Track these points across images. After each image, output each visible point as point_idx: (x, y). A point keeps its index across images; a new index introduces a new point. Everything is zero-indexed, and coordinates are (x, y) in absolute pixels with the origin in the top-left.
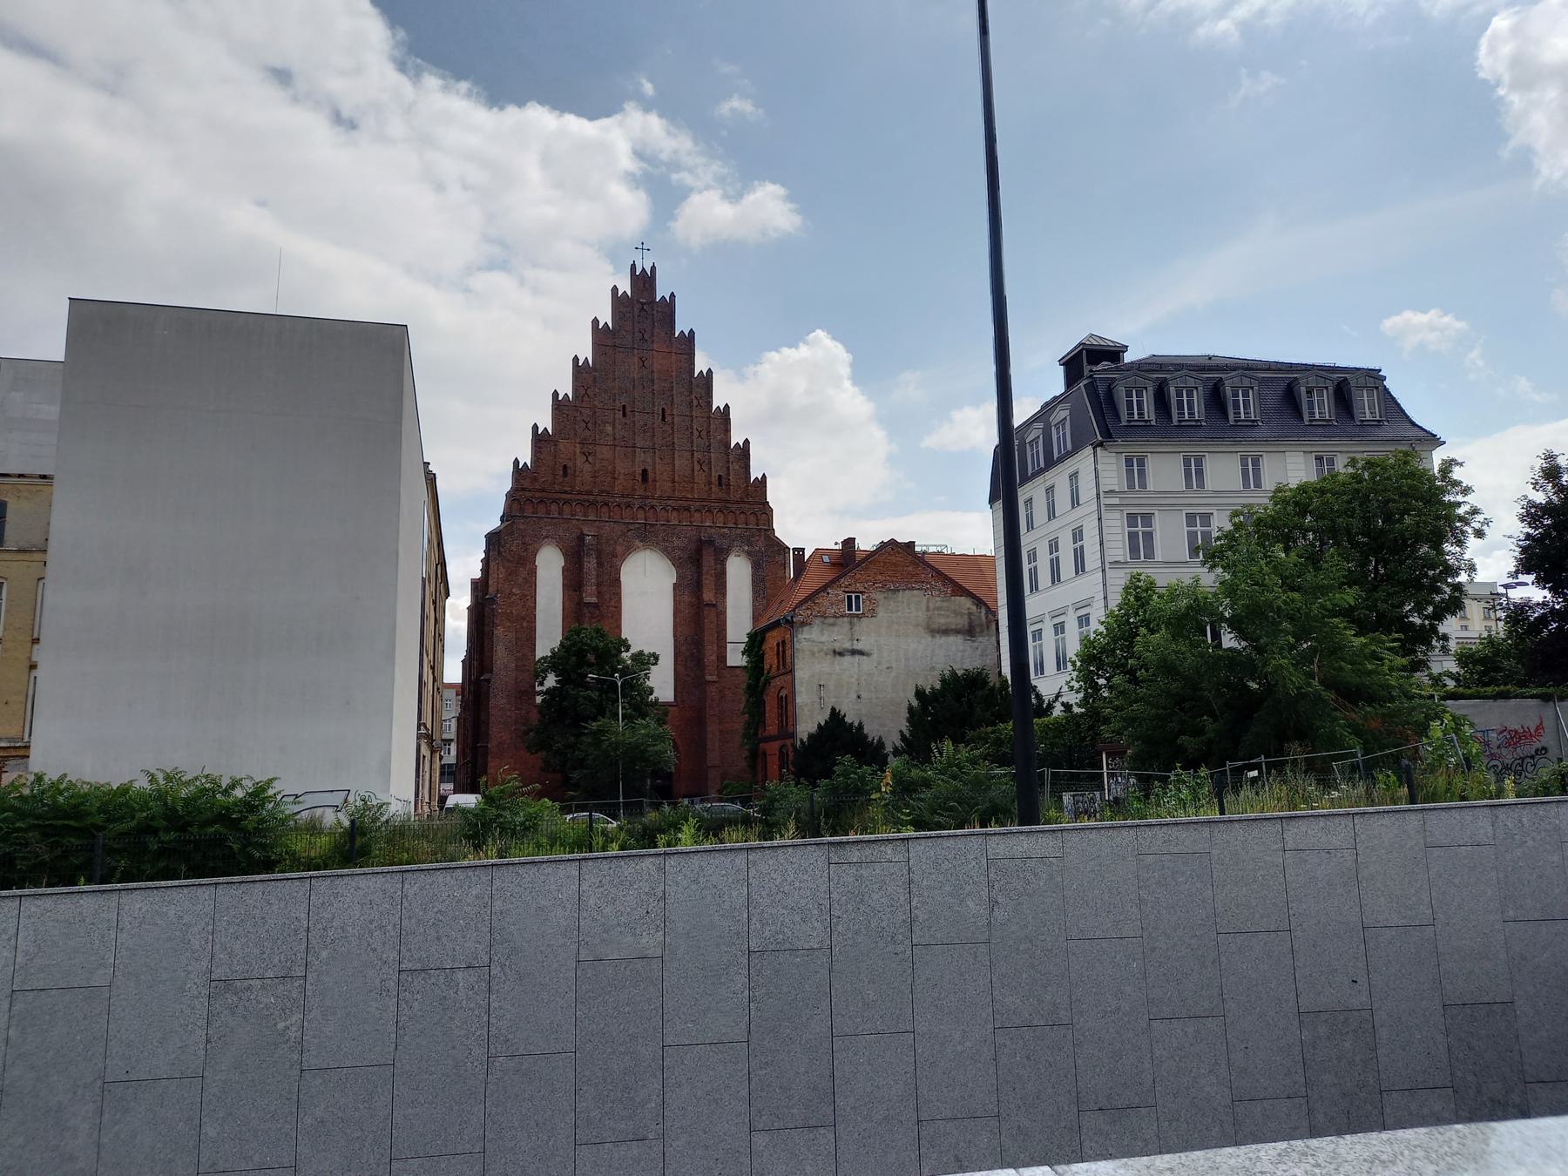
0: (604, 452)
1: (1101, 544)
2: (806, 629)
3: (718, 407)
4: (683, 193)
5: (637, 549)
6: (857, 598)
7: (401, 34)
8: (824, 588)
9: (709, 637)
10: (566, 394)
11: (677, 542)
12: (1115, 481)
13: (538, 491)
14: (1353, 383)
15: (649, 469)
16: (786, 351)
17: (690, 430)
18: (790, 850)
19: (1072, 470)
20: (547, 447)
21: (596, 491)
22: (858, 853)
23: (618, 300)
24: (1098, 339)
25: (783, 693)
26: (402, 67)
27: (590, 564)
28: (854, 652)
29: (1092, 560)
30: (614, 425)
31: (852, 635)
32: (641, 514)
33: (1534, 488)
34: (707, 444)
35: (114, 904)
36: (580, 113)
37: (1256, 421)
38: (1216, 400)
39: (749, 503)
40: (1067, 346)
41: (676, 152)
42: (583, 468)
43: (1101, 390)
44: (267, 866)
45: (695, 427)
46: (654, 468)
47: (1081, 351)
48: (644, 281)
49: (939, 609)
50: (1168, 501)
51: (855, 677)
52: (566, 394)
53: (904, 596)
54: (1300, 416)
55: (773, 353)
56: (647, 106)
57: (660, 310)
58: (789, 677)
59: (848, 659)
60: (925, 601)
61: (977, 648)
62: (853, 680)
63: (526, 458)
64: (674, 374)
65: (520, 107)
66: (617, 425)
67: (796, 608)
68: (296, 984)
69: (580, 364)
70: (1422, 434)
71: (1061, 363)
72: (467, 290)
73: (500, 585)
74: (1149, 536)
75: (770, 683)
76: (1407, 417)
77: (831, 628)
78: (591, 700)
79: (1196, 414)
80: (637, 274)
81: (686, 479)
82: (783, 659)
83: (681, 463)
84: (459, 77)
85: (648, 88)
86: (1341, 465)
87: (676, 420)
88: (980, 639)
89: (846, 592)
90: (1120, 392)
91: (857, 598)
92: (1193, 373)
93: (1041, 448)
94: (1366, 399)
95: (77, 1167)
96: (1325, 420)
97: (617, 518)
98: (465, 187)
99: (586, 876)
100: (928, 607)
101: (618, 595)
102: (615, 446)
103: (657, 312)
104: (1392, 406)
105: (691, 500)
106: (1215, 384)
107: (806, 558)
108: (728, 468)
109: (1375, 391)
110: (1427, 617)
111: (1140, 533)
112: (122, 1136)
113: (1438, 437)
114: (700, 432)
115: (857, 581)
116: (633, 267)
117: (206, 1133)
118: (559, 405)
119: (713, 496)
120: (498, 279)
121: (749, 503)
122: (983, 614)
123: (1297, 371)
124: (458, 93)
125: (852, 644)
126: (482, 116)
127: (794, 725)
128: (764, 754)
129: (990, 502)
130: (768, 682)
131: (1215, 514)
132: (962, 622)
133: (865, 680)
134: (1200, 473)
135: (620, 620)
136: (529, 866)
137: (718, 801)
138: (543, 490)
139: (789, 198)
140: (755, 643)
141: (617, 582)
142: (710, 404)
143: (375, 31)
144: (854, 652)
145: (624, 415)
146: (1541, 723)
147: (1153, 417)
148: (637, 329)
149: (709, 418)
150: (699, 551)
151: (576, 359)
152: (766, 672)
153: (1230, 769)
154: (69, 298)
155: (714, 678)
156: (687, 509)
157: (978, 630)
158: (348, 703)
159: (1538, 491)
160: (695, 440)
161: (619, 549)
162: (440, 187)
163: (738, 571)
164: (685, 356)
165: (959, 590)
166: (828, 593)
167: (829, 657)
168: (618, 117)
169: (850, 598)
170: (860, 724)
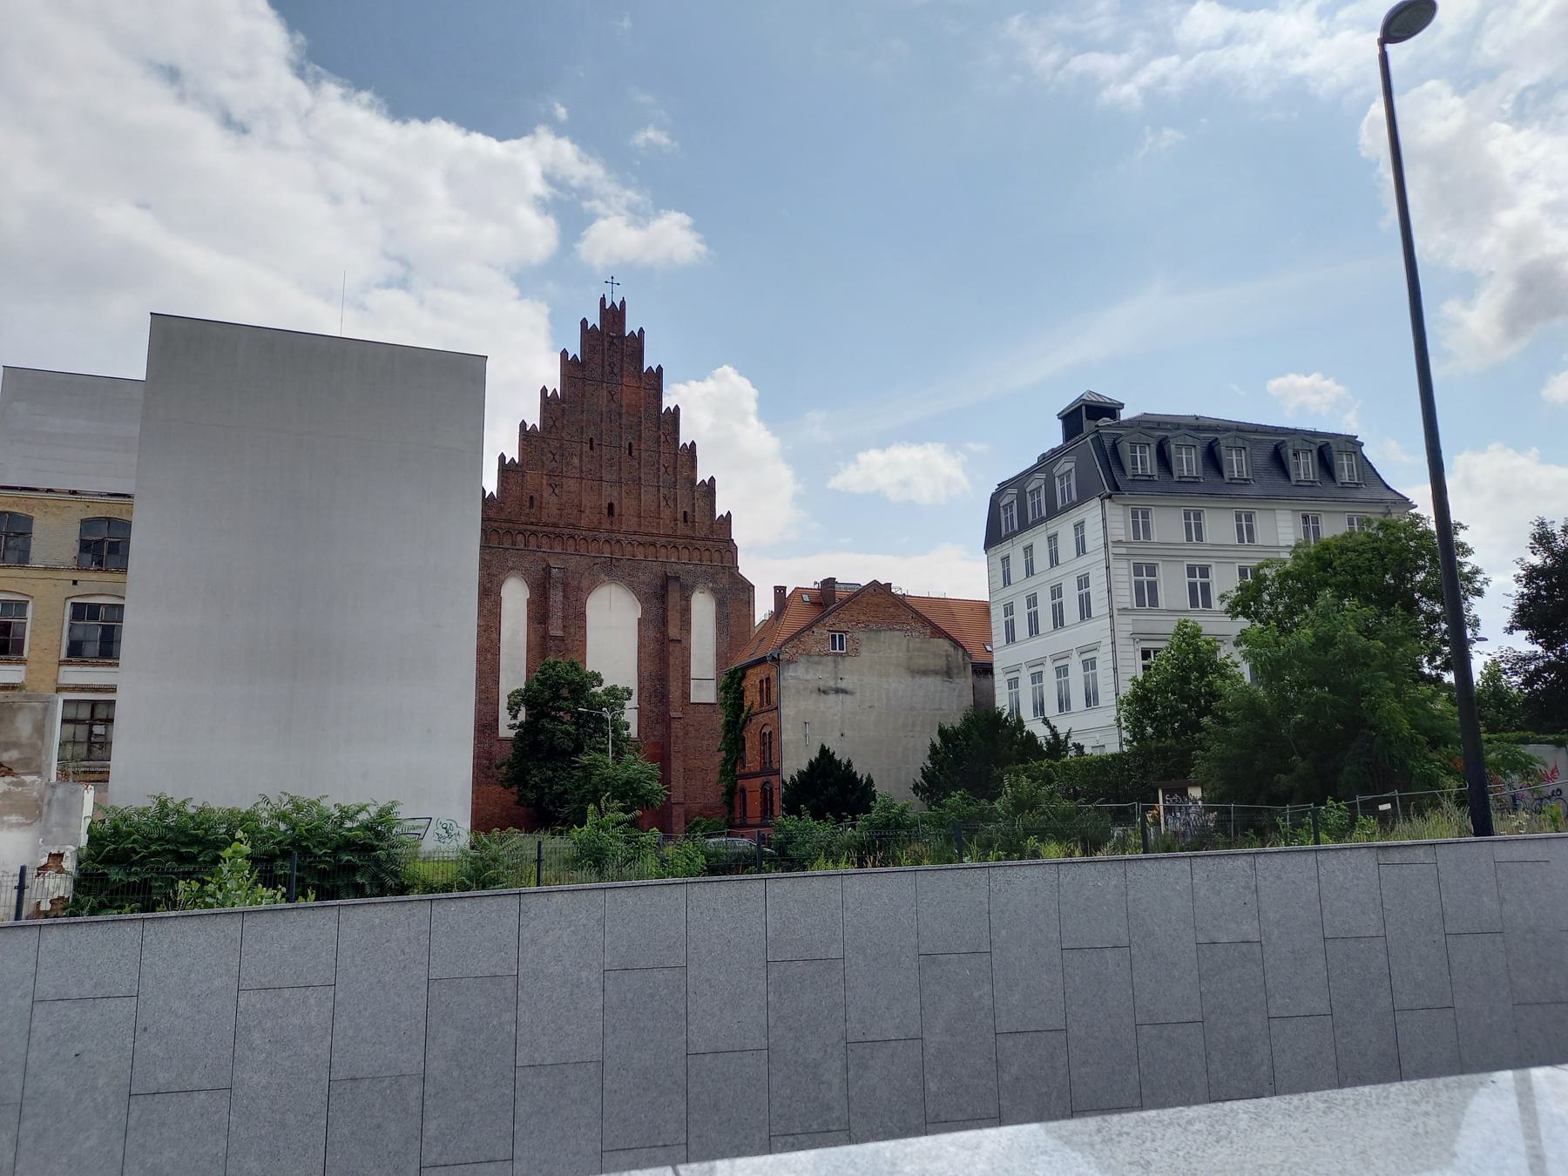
0: (571, 485)
1: (1109, 591)
2: (792, 666)
3: (685, 444)
4: (591, 218)
6: (841, 637)
7: (300, 38)
8: (809, 627)
9: (674, 675)
12: (1123, 532)
13: (506, 521)
14: (1334, 447)
17: (657, 466)
18: (1348, 852)
19: (1077, 520)
22: (1398, 855)
24: (1096, 396)
25: (766, 730)
26: (300, 72)
27: (556, 597)
28: (838, 691)
29: (1099, 605)
30: (581, 457)
32: (607, 548)
33: (1533, 552)
34: (673, 479)
35: (839, 887)
36: (488, 132)
37: (1249, 480)
38: (1212, 459)
40: (1066, 401)
41: (587, 179)
42: (551, 500)
43: (1108, 444)
44: (403, 890)
48: (613, 315)
49: (919, 650)
50: (1171, 553)
51: (839, 715)
53: (885, 636)
54: (1288, 477)
55: (682, 386)
56: (559, 131)
58: (775, 714)
59: (832, 697)
60: (905, 641)
61: (954, 690)
62: (836, 718)
64: (642, 409)
66: (584, 457)
67: (782, 645)
68: (985, 959)
69: (549, 395)
70: (1397, 498)
71: (1060, 416)
72: (362, 307)
74: (1153, 587)
75: (751, 720)
76: (1383, 481)
78: (568, 733)
80: (607, 307)
81: (652, 515)
82: (767, 696)
83: (648, 498)
84: (359, 85)
85: (561, 112)
88: (957, 680)
92: (1192, 432)
93: (1043, 497)
94: (1345, 462)
95: (834, 1115)
96: (1193, 477)
98: (364, 200)
99: (1197, 871)
100: (908, 647)
104: (1368, 473)
105: (657, 535)
106: (1276, 446)
107: (787, 596)
109: (1243, 451)
110: (1436, 668)
112: (866, 1090)
113: (1410, 501)
114: (666, 468)
115: (841, 620)
116: (603, 300)
117: (928, 1089)
120: (395, 296)
122: (960, 656)
123: (1283, 434)
125: (836, 683)
126: (384, 129)
127: (780, 761)
128: (743, 790)
129: (985, 548)
130: (749, 718)
131: (1160, 565)
132: (941, 663)
133: (849, 718)
134: (1250, 530)
135: (585, 654)
136: (1152, 861)
138: (510, 521)
139: (695, 228)
140: (732, 683)
141: (582, 616)
142: (677, 440)
143: (272, 34)
144: (838, 691)
145: (591, 448)
146: (1556, 766)
147: (1155, 472)
148: (607, 363)
149: (676, 454)
150: (665, 587)
151: (544, 390)
152: (746, 709)
153: (1360, 802)
154: (151, 313)
155: (679, 715)
156: (653, 544)
157: (955, 671)
158: (429, 731)
159: (1535, 554)
161: (585, 583)
162: (335, 199)
163: (703, 608)
165: (938, 632)
167: (814, 694)
168: (527, 139)
169: (834, 637)
170: (849, 761)
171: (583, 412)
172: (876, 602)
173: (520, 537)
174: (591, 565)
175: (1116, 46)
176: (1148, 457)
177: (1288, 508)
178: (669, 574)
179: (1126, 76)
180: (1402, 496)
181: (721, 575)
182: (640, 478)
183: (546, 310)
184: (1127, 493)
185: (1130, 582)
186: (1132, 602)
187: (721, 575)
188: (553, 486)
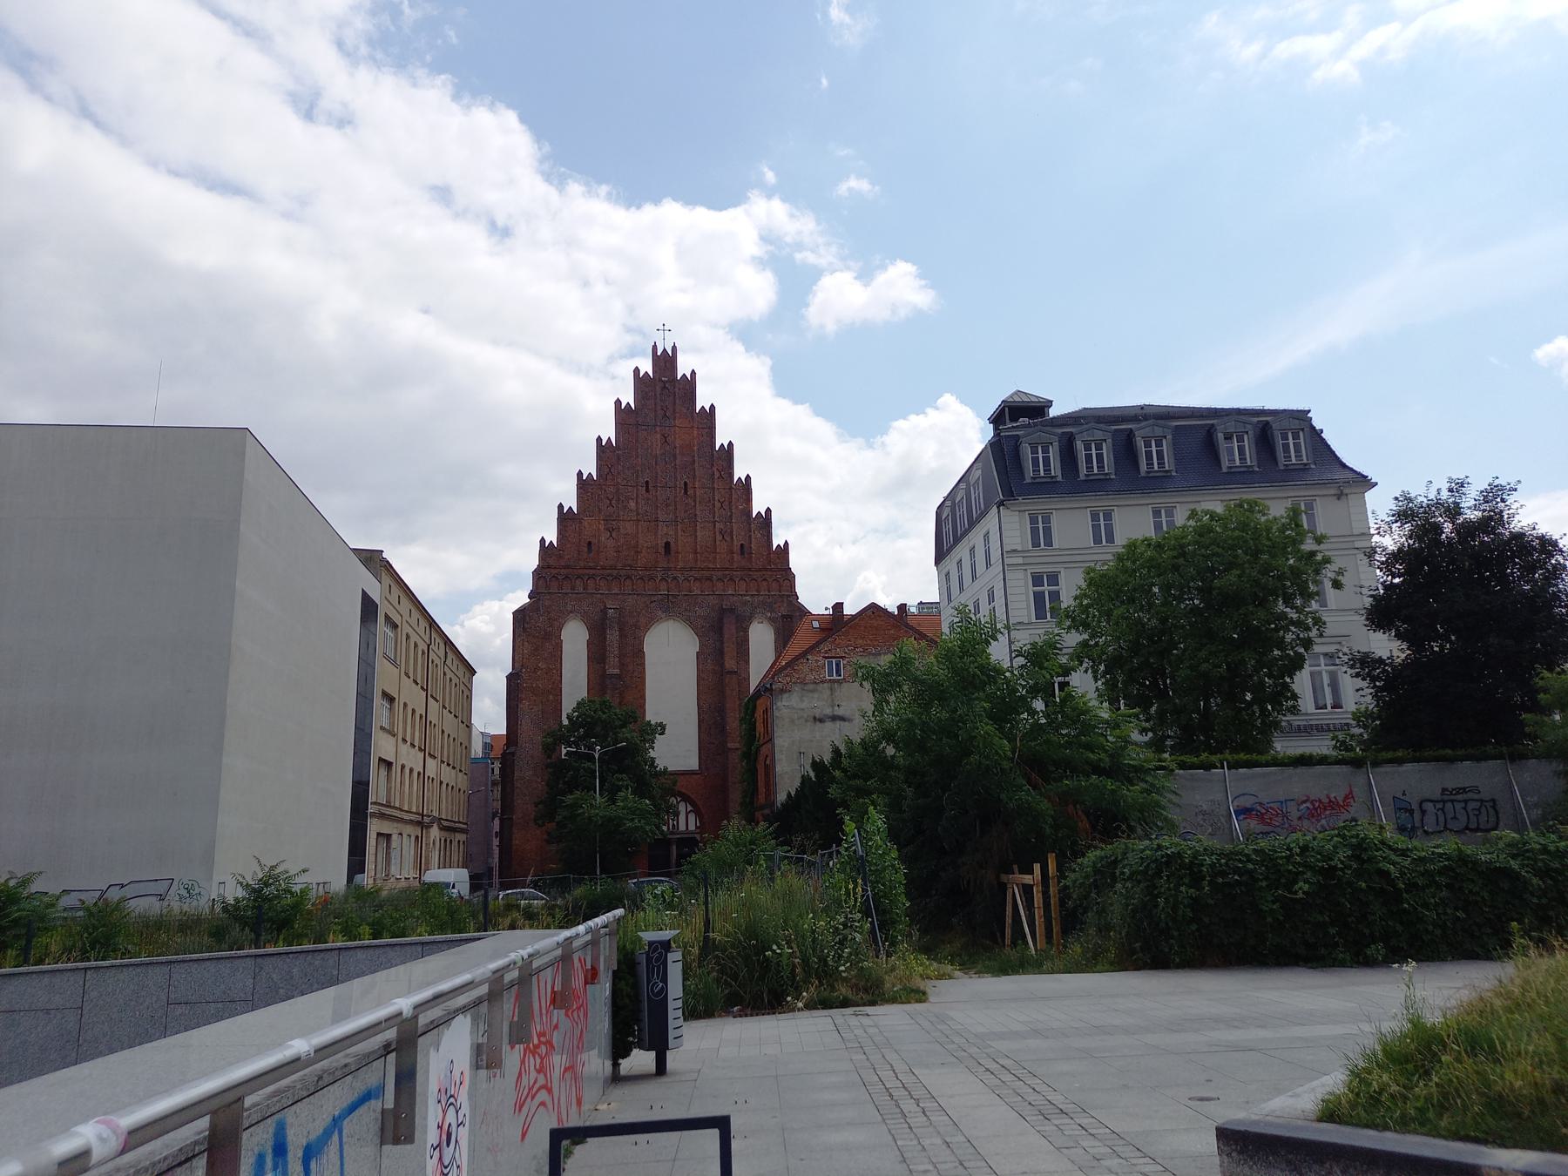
2: (785, 696)
5: (660, 620)
6: (838, 665)
7: (547, 148)
10: (590, 473)
13: (565, 567)
15: (672, 542)
16: (913, 417)
20: (571, 526)
21: (619, 565)
23: (640, 381)
26: (548, 177)
27: (613, 636)
28: (834, 718)
31: (833, 700)
32: (663, 585)
37: (1252, 466)
38: (1126, 450)
39: (771, 570)
45: (716, 498)
46: (676, 540)
47: (1003, 409)
48: (665, 361)
52: (590, 473)
57: (681, 387)
58: (769, 745)
59: (829, 725)
63: (552, 537)
65: (656, 205)
69: (603, 444)
70: (1351, 475)
73: (524, 660)
77: (811, 695)
79: (1248, 459)
85: (770, 177)
86: (1180, 518)
89: (826, 658)
90: (1026, 450)
91: (838, 665)
96: (1246, 467)
98: (607, 282)
101: (643, 664)
102: (639, 520)
103: (679, 389)
105: (713, 569)
106: (1208, 431)
108: (750, 536)
113: (1369, 478)
116: (655, 347)
118: (583, 484)
121: (771, 570)
124: (598, 196)
126: (621, 217)
134: (1048, 531)
137: (645, 876)
138: (567, 567)
141: (640, 654)
142: (731, 475)
144: (834, 718)
145: (647, 491)
149: (731, 488)
150: (721, 620)
156: (709, 579)
160: (717, 511)
162: (586, 284)
164: (706, 430)
166: (808, 659)
167: (809, 724)
172: (875, 625)
173: (578, 582)
174: (648, 602)
175: (1326, 25)
176: (1302, 444)
177: (1214, 498)
178: (724, 607)
179: (1340, 53)
180: (1359, 474)
182: (696, 515)
183: (769, 362)
184: (1020, 498)
185: (1027, 594)
186: (1029, 615)
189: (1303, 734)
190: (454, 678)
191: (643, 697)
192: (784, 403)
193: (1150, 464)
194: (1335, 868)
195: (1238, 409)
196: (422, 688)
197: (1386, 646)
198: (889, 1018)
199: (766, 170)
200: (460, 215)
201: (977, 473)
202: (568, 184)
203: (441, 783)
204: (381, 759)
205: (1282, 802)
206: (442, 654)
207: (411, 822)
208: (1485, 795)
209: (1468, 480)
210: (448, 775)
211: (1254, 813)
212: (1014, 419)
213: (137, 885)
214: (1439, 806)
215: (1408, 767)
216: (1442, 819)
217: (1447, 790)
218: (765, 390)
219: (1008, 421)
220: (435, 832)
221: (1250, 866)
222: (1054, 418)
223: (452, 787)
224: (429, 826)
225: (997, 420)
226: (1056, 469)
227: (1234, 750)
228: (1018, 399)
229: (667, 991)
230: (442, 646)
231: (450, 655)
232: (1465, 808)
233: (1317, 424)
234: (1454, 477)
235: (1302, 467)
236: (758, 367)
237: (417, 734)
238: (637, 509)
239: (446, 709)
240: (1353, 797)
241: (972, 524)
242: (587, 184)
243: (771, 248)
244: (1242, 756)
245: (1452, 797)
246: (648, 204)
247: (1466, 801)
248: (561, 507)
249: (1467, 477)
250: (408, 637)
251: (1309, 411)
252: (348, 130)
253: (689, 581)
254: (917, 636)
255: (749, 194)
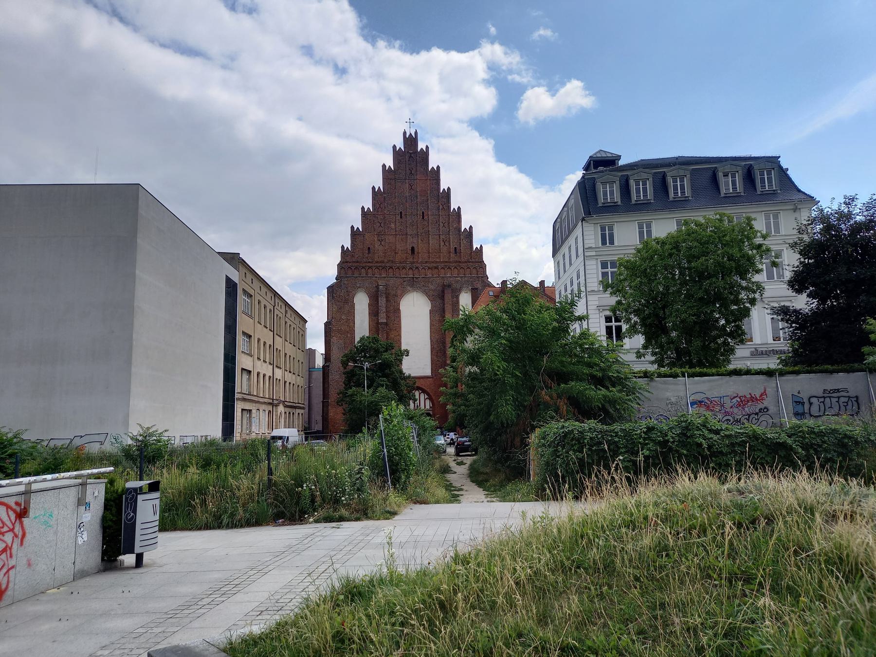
7: (365, 21)
11: (432, 287)
12: (593, 241)
13: (354, 262)
15: (415, 246)
21: (386, 261)
23: (397, 153)
26: (366, 38)
27: (382, 301)
32: (411, 272)
46: (418, 246)
63: (348, 245)
65: (428, 51)
70: (803, 196)
85: (493, 30)
87: (430, 218)
92: (646, 170)
94: (608, 189)
97: (398, 275)
98: (401, 98)
101: (399, 317)
111: (610, 272)
118: (365, 214)
119: (451, 260)
126: (407, 59)
138: (357, 262)
141: (397, 311)
142: (449, 207)
145: (401, 217)
147: (742, 191)
150: (443, 292)
151: (373, 188)
161: (399, 292)
162: (389, 99)
168: (476, 51)
171: (395, 198)
180: (808, 195)
181: (477, 282)
183: (493, 142)
184: (594, 216)
185: (597, 273)
187: (477, 282)
188: (380, 241)
189: (764, 356)
190: (291, 323)
191: (400, 335)
192: (502, 166)
193: (676, 193)
194: (668, 441)
195: (735, 157)
196: (270, 330)
197: (802, 303)
198: (385, 526)
199: (490, 26)
200: (319, 62)
201: (572, 201)
202: (377, 41)
203: (285, 382)
204: (243, 369)
205: (721, 397)
206: (283, 311)
207: (265, 403)
208: (852, 393)
209: (857, 196)
210: (289, 377)
211: (703, 403)
212: (596, 167)
213: (88, 436)
214: (822, 400)
215: (802, 376)
216: (822, 408)
217: (827, 390)
218: (491, 159)
219: (592, 169)
220: (281, 408)
221: (616, 439)
222: (621, 166)
223: (293, 385)
224: (277, 405)
225: (587, 168)
226: (617, 198)
227: (692, 366)
228: (599, 155)
229: (136, 518)
230: (283, 307)
231: (289, 312)
232: (838, 402)
233: (784, 165)
234: (848, 195)
235: (772, 192)
236: (487, 145)
237: (268, 355)
238: (396, 228)
239: (287, 341)
240: (766, 395)
241: (570, 232)
242: (389, 41)
243: (494, 73)
244: (698, 369)
245: (830, 395)
246: (423, 51)
247: (839, 397)
248: (352, 227)
249: (856, 195)
250: (259, 302)
251: (780, 157)
252: (255, 15)
253: (425, 270)
254: (548, 299)
255: (481, 42)
